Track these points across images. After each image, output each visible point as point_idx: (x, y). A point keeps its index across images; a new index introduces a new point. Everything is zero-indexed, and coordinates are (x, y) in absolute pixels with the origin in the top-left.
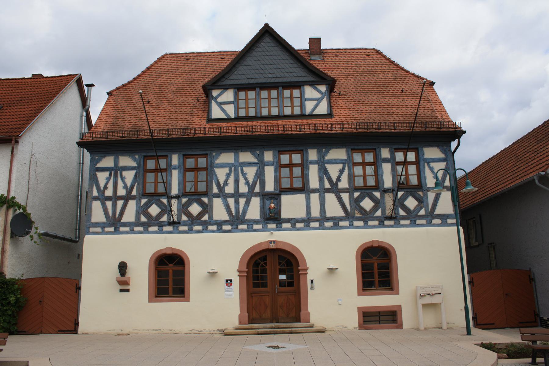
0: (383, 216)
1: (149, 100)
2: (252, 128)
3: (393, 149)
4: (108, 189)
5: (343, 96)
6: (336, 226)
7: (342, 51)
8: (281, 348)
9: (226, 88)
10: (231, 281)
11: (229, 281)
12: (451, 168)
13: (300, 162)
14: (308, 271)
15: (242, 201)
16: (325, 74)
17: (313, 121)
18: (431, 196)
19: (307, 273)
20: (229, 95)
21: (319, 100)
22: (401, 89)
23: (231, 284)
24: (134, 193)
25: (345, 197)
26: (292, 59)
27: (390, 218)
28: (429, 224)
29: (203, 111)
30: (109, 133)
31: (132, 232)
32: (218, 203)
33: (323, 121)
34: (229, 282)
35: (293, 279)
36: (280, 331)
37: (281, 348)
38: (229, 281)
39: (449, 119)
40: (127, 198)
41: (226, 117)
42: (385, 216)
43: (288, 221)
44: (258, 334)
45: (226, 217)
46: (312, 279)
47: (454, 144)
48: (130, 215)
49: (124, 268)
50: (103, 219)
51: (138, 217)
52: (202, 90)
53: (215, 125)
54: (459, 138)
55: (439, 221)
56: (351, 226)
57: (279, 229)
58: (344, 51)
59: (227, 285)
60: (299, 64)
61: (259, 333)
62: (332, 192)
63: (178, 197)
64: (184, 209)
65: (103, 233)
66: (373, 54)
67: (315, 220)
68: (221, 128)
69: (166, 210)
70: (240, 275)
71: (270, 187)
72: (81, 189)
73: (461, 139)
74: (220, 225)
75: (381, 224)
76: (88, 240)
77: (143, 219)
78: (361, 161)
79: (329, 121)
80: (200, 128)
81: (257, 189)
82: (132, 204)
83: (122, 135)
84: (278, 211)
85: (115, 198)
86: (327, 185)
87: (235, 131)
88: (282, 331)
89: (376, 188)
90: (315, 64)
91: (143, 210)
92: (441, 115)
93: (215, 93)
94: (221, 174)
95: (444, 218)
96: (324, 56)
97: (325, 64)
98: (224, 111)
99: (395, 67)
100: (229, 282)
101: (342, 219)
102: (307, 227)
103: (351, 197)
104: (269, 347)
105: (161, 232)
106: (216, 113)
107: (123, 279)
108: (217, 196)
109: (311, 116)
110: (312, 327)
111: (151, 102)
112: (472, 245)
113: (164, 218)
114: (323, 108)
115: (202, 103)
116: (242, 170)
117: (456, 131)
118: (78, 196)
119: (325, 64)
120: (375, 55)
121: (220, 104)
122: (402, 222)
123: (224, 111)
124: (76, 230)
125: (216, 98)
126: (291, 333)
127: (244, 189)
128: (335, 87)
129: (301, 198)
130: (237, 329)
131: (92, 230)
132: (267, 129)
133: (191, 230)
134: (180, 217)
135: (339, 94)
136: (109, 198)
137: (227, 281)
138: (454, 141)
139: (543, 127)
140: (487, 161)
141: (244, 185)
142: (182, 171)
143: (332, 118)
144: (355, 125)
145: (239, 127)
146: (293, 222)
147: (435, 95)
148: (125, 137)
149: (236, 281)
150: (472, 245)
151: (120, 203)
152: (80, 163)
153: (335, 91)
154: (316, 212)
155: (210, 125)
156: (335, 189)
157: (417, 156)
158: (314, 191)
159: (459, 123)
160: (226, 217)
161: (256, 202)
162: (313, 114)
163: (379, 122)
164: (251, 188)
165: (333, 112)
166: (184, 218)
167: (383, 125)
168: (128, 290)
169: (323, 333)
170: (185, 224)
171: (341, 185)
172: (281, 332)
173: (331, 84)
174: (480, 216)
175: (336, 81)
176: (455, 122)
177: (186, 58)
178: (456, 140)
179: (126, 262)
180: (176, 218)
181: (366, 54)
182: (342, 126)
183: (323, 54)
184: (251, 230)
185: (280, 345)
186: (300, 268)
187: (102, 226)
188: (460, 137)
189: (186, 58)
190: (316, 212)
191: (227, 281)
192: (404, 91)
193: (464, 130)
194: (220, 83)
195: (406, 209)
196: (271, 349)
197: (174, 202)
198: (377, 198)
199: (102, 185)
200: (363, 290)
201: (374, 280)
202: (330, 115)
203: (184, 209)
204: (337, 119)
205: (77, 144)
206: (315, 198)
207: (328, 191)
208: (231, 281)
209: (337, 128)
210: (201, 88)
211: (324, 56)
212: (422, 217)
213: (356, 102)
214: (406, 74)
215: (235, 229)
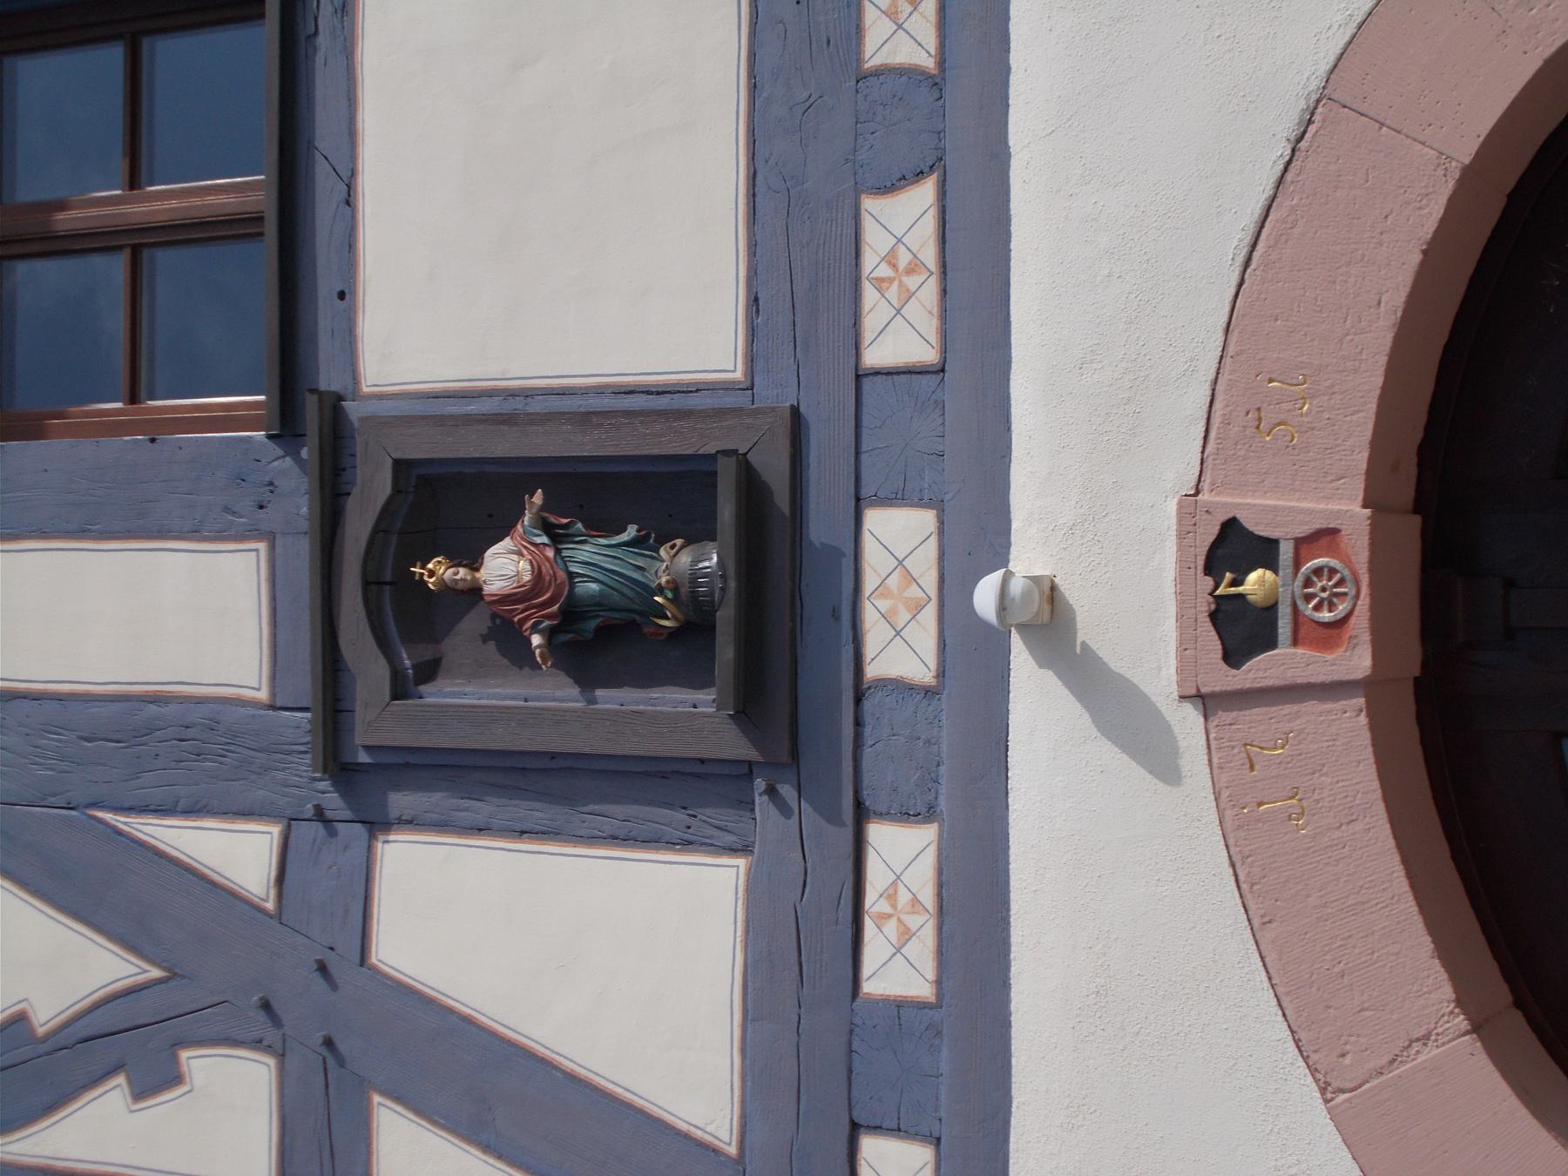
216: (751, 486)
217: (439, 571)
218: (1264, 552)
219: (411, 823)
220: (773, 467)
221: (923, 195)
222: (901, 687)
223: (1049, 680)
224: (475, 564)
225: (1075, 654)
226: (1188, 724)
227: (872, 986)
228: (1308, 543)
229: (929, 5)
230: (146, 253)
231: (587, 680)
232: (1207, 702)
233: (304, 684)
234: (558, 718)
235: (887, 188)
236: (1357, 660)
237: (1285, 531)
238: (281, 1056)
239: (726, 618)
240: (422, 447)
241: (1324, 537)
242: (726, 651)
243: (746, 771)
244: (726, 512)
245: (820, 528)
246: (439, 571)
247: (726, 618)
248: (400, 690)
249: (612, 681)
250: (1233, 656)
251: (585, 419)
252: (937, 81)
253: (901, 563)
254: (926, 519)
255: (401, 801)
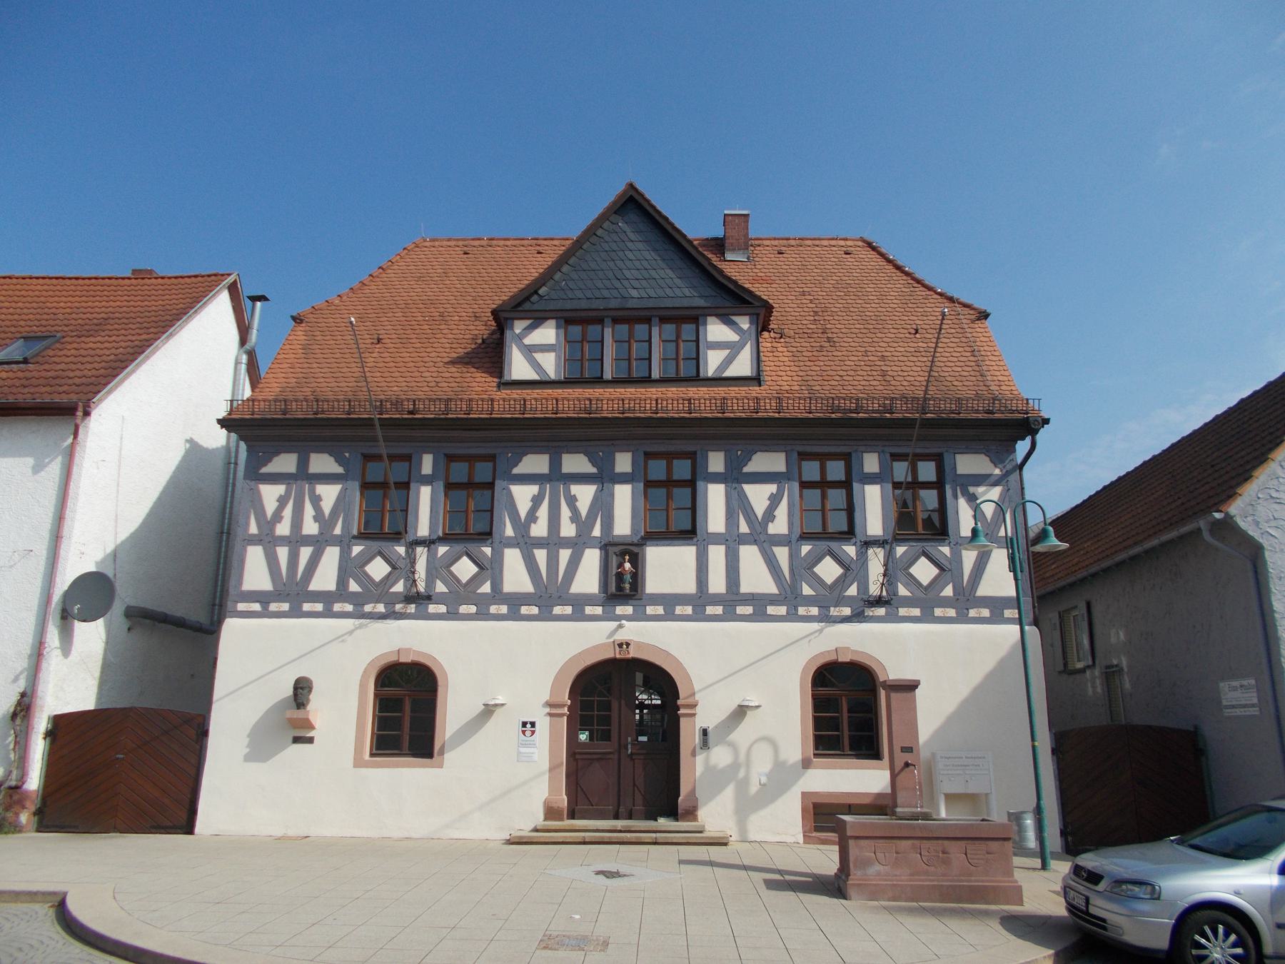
0: (860, 596)
1: (381, 337)
2: (591, 404)
3: (888, 456)
4: (539, 521)
5: (787, 340)
6: (760, 616)
7: (793, 242)
8: (625, 875)
9: (538, 320)
10: (533, 724)
11: (529, 726)
12: (1017, 502)
13: (844, 479)
14: (698, 709)
15: (565, 555)
16: (751, 293)
17: (720, 391)
18: (969, 558)
19: (694, 715)
20: (547, 334)
21: (734, 349)
22: (914, 327)
23: (533, 732)
24: (338, 531)
25: (782, 554)
26: (682, 259)
27: (879, 602)
28: (962, 618)
29: (494, 363)
30: (320, 403)
31: (328, 613)
32: (513, 558)
33: (742, 391)
34: (528, 726)
35: (609, 725)
36: (631, 838)
37: (625, 875)
38: (529, 726)
39: (1015, 392)
40: (319, 543)
41: (536, 377)
42: (865, 597)
43: (657, 599)
44: (584, 843)
45: (528, 587)
46: (705, 726)
47: (1022, 447)
48: (325, 578)
49: (306, 691)
50: (265, 584)
51: (342, 582)
52: (491, 318)
53: (516, 393)
54: (1034, 432)
55: (748, 610)
56: (792, 617)
57: (639, 616)
58: (798, 242)
59: (524, 732)
60: (697, 271)
61: (587, 840)
62: (755, 542)
63: (429, 543)
64: (439, 569)
65: (265, 614)
66: (859, 249)
67: (716, 599)
68: (525, 400)
69: (402, 569)
70: (552, 712)
71: (623, 526)
72: (230, 519)
73: (1038, 437)
74: (515, 603)
75: (858, 617)
76: (232, 630)
77: (354, 587)
78: (817, 478)
79: (755, 391)
80: (483, 400)
81: (597, 532)
82: (332, 556)
83: (318, 408)
84: (637, 578)
85: (553, 542)
86: (744, 528)
87: (555, 409)
88: (637, 838)
89: (849, 533)
90: (730, 270)
91: (347, 569)
92: (997, 383)
93: (519, 326)
94: (523, 495)
95: (996, 607)
96: (755, 252)
97: (754, 270)
98: (537, 366)
99: (905, 278)
100: (528, 726)
101: (773, 600)
102: (699, 616)
103: (793, 556)
104: (598, 873)
105: (390, 615)
106: (519, 368)
107: (299, 714)
108: (511, 543)
109: (718, 381)
110: (701, 832)
111: (383, 341)
112: (1070, 667)
113: (399, 587)
114: (742, 366)
115: (491, 345)
116: (312, 492)
117: (1028, 417)
118: (222, 533)
119: (754, 270)
120: (863, 252)
121: (529, 351)
122: (903, 612)
123: (537, 366)
124: (214, 605)
125: (520, 338)
126: (655, 843)
127: (568, 529)
128: (770, 320)
129: (685, 554)
130: (536, 830)
131: (241, 607)
132: (621, 405)
133: (452, 615)
134: (430, 581)
135: (779, 336)
136: (540, 543)
137: (524, 724)
138: (1023, 439)
139: (1235, 411)
140: (1112, 483)
141: (311, 520)
142: (641, 485)
143: (760, 386)
144: (831, 402)
145: (563, 399)
146: (670, 602)
147: (987, 339)
148: (323, 412)
149: (543, 725)
150: (1070, 667)
151: (305, 553)
152: (230, 463)
153: (773, 329)
154: (717, 584)
155: (505, 393)
156: (760, 537)
157: (940, 470)
158: (717, 539)
159: (1036, 402)
160: (528, 587)
161: (592, 559)
162: (728, 374)
163: (892, 396)
164: (584, 526)
165: (765, 373)
166: (440, 587)
167: (867, 404)
168: (310, 740)
169: (725, 847)
170: (441, 599)
171: (773, 529)
172: (633, 840)
173: (762, 314)
174: (1089, 605)
175: (773, 308)
176: (1027, 400)
177: (465, 249)
178: (1028, 439)
179: (312, 678)
180: (421, 587)
181: (845, 249)
182: (779, 403)
183: (752, 248)
184: (579, 616)
185: (622, 870)
186: (679, 702)
187: (262, 598)
188: (1036, 431)
189: (465, 249)
190: (717, 584)
191: (524, 724)
192: (919, 331)
193: (1046, 417)
194: (527, 306)
195: (913, 582)
196: (601, 877)
197: (421, 552)
198: (447, 551)
199: (523, 511)
200: (814, 754)
201: (817, 733)
202: (756, 379)
203: (439, 569)
204: (771, 388)
205: (222, 427)
206: (717, 555)
207: (743, 539)
208: (533, 724)
209: (736, 408)
210: (490, 314)
211: (755, 252)
212: (946, 603)
213: (814, 353)
214: (928, 293)
215: (546, 615)
216: (634, 595)
217: (627, 557)
218: (627, 648)
219: (601, 554)
220: (636, 597)
221: (663, 613)
222: (615, 610)
223: (615, 626)
224: (628, 562)
225: (260, 468)
226: (612, 640)
227: (586, 607)
228: (628, 651)
229: (2, 905)
230: (695, 375)
231: (615, 575)
232: (614, 642)
233: (616, 540)
234: (612, 571)
235: (664, 609)
236: (618, 656)
237: (629, 649)
238: (575, 537)
239: (621, 593)
240: (640, 556)
241: (629, 653)
242: (618, 593)
243: (607, 594)
244: (632, 593)
245: (630, 602)
246: (627, 557)
247: (621, 593)
248: (615, 553)
249: (616, 578)
250: (618, 644)
251: (642, 572)
252: (674, 614)
253: (582, 342)
254: (631, 613)
255: (603, 552)
